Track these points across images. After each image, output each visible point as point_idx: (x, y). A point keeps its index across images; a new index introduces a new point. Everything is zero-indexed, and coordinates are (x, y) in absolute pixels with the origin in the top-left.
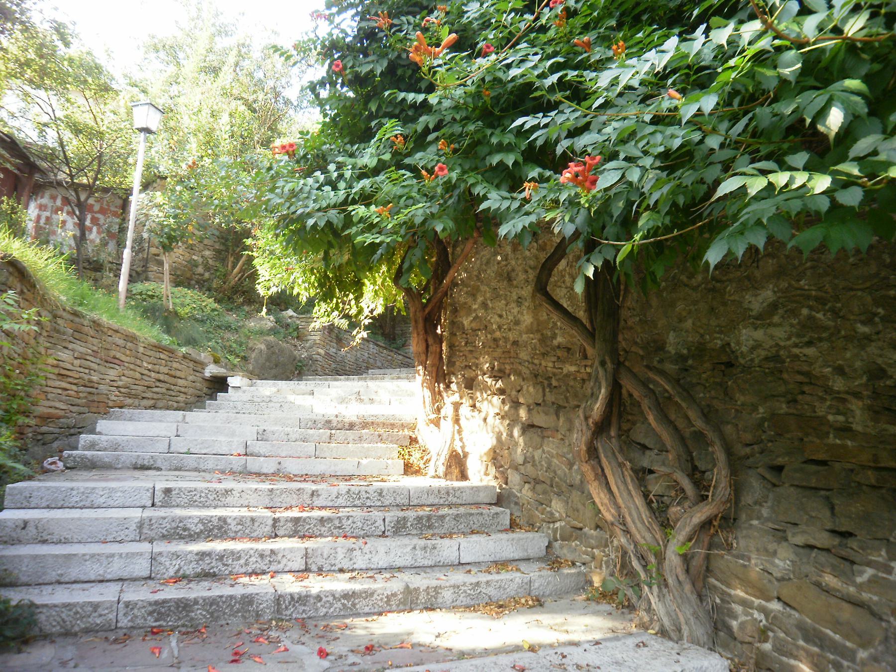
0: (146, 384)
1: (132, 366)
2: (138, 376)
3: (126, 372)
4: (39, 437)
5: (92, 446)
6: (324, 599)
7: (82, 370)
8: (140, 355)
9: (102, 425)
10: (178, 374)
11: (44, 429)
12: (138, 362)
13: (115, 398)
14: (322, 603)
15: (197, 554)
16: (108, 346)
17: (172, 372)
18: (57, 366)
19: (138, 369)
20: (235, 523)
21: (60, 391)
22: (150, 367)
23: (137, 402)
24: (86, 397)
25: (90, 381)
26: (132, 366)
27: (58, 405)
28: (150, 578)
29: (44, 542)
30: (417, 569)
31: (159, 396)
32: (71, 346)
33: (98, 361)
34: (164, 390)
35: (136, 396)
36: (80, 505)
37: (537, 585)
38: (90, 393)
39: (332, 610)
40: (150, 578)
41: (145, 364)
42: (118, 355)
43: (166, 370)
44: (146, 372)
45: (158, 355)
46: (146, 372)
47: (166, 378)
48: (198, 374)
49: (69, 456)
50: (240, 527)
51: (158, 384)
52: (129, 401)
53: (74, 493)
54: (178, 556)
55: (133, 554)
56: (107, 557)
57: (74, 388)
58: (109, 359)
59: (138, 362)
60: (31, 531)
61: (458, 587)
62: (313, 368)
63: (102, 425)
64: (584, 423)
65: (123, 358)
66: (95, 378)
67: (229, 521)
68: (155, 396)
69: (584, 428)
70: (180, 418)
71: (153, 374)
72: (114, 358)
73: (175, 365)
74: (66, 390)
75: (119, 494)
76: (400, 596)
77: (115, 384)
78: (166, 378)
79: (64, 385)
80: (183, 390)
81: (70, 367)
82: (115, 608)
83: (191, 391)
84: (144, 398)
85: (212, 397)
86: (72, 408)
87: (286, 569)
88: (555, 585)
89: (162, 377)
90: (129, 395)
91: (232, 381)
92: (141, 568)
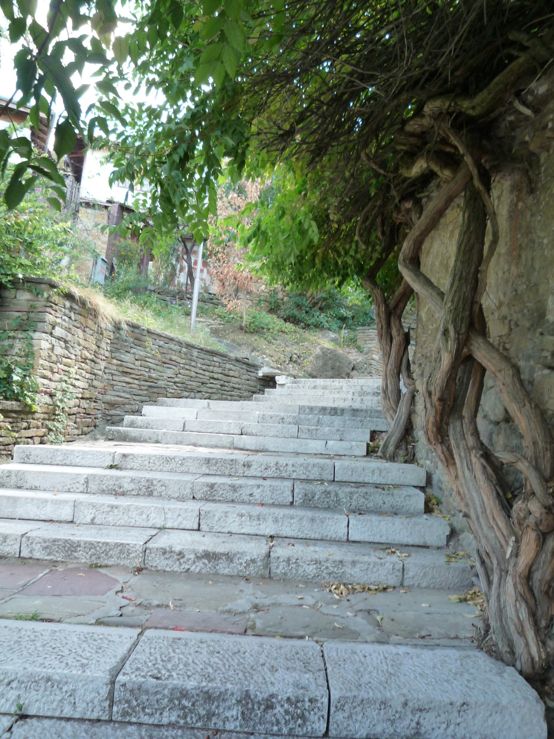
0: (201, 380)
1: (187, 367)
2: (193, 374)
3: (182, 371)
4: (109, 418)
5: (132, 425)
6: (187, 556)
7: (142, 368)
8: (194, 358)
9: (147, 409)
10: (231, 373)
11: (113, 412)
12: (193, 364)
13: (173, 391)
14: (185, 560)
15: (108, 506)
16: (165, 351)
17: (226, 372)
18: (121, 366)
19: (193, 369)
20: (160, 484)
21: (124, 385)
22: (204, 367)
23: (192, 395)
24: (146, 390)
25: (150, 377)
26: (187, 367)
27: (122, 394)
28: (72, 522)
29: (19, 488)
30: (306, 540)
31: (214, 390)
32: (133, 351)
33: (157, 362)
34: (219, 386)
35: (192, 390)
36: (63, 463)
37: (411, 574)
38: (150, 387)
39: (194, 567)
40: (72, 522)
41: (199, 365)
42: (174, 358)
43: (220, 370)
44: (201, 371)
45: (211, 358)
46: (201, 371)
47: (220, 376)
48: (252, 374)
49: (110, 430)
50: (163, 488)
51: (212, 381)
52: (186, 394)
53: (59, 453)
54: (94, 506)
55: (61, 501)
56: (42, 502)
57: (136, 382)
58: (166, 361)
59: (193, 364)
60: (13, 479)
61: (320, 563)
62: (368, 370)
63: (147, 409)
64: (428, 400)
65: (179, 360)
66: (154, 375)
67: (155, 482)
68: (210, 391)
69: (428, 405)
70: (206, 405)
71: (207, 373)
72: (171, 360)
73: (228, 366)
74: (129, 383)
75: (89, 456)
76: (259, 564)
77: (172, 380)
78: (220, 376)
79: (128, 379)
80: (237, 386)
81: (133, 366)
82: (19, 540)
83: (245, 387)
84: (199, 392)
85: (262, 391)
86: (135, 397)
87: (181, 527)
88: (433, 578)
89: (216, 376)
90: (186, 389)
91: (280, 380)
92: (66, 513)
